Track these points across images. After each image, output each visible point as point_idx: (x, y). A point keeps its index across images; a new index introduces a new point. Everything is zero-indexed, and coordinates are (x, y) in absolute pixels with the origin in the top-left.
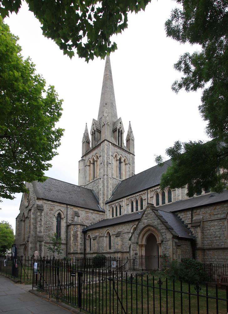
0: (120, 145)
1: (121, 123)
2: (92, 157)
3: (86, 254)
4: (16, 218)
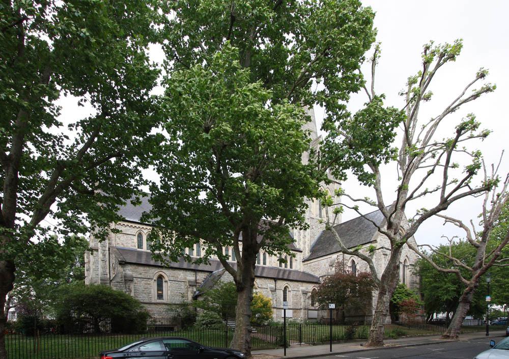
3: (275, 281)
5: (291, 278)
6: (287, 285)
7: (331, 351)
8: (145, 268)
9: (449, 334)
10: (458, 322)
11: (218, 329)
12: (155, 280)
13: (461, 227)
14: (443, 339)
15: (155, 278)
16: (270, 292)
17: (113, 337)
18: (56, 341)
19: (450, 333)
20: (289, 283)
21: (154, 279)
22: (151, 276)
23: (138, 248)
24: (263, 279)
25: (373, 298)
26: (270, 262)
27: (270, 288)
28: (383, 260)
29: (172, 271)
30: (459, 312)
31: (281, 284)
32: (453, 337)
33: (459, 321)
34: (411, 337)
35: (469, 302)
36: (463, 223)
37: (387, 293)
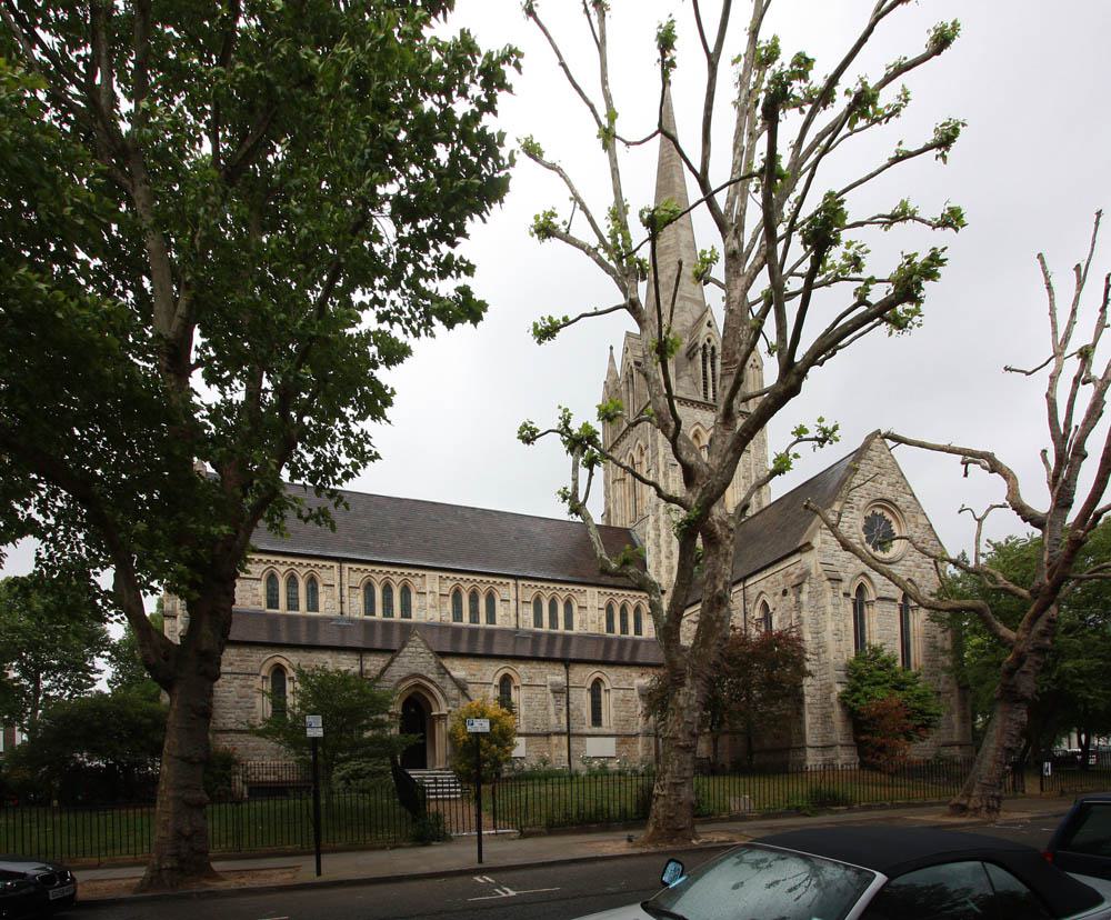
0: (711, 396)
1: (712, 323)
2: (758, 597)
3: (567, 667)
4: (1101, 414)
5: (640, 660)
6: (506, 671)
7: (480, 861)
8: (242, 651)
9: (965, 802)
10: (991, 764)
11: (368, 792)
12: (263, 677)
13: (992, 471)
14: (950, 815)
15: (496, 682)
16: (551, 695)
17: (145, 810)
18: (65, 818)
19: (969, 796)
20: (605, 670)
21: (263, 673)
22: (256, 666)
23: (268, 607)
24: (534, 664)
25: (808, 700)
26: (582, 622)
27: (551, 685)
28: (830, 594)
29: (306, 654)
30: (994, 731)
31: (584, 675)
32: (976, 810)
33: (996, 762)
34: (868, 808)
35: (1023, 699)
36: (998, 457)
37: (688, 681)
